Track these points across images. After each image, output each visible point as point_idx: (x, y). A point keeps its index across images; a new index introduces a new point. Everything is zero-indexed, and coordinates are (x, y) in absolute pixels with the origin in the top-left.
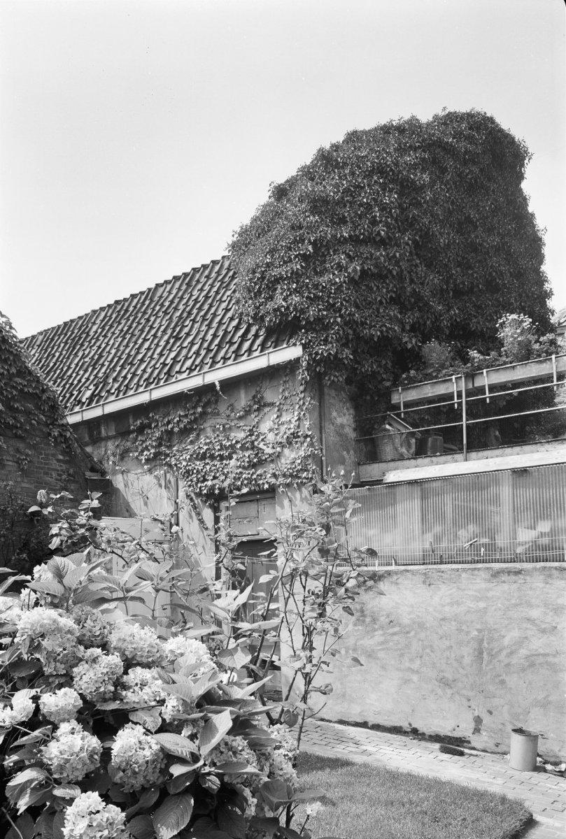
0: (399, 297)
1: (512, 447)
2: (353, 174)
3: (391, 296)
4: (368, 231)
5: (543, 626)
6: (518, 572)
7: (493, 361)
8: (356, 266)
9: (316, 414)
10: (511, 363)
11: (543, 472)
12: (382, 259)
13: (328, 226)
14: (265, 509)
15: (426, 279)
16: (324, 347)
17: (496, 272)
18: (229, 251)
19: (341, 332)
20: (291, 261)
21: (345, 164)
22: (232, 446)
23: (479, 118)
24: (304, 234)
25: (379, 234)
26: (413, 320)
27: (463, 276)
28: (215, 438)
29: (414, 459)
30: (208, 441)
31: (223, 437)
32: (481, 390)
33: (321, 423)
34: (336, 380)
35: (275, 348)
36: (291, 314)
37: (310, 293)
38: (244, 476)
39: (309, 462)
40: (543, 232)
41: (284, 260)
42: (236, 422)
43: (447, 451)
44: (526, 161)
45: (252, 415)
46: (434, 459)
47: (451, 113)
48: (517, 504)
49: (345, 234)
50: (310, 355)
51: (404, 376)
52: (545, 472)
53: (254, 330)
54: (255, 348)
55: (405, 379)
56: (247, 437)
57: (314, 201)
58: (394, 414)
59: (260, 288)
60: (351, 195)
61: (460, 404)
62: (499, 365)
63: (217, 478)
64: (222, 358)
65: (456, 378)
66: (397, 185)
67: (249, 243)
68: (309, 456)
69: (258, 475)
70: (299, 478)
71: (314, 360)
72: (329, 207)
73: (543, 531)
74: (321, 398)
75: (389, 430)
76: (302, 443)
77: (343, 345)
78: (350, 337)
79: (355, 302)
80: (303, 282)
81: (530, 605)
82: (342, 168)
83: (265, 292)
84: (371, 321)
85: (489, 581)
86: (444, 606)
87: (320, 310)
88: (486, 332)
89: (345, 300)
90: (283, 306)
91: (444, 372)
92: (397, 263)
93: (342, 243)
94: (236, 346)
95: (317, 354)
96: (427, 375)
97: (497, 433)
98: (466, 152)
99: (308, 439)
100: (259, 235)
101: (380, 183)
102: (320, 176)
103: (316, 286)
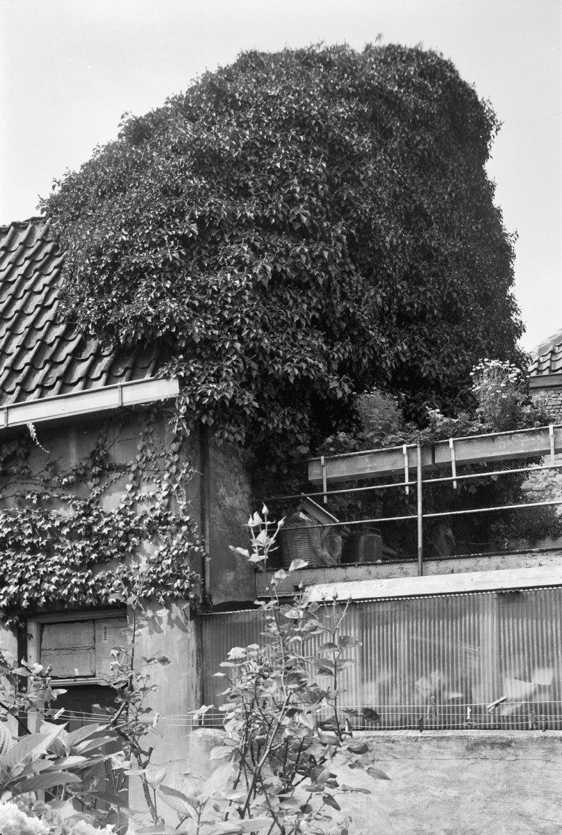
0: (324, 317)
1: (489, 556)
2: (258, 121)
3: (314, 316)
4: (282, 213)
5: (542, 825)
6: (506, 744)
7: (464, 427)
8: (264, 266)
9: (196, 489)
10: (489, 431)
11: (542, 596)
12: (304, 258)
13: (221, 197)
14: (109, 640)
15: (363, 295)
16: (215, 386)
17: (458, 294)
18: (43, 211)
19: (241, 365)
20: (162, 243)
21: (246, 105)
22: (55, 532)
23: (432, 61)
24: (184, 205)
25: (298, 219)
26: (343, 355)
27: (410, 295)
28: (23, 516)
29: (343, 567)
30: (11, 519)
31: (38, 515)
32: (445, 469)
33: (202, 504)
34: (231, 438)
35: (130, 379)
36: (161, 328)
37: (193, 298)
38: (73, 581)
39: (185, 565)
40: (513, 239)
41: (151, 242)
42: (60, 491)
43: (388, 559)
44: (493, 133)
45: (89, 483)
46: (372, 568)
47: (393, 46)
48: (505, 643)
49: (249, 214)
50: (192, 396)
51: (329, 440)
52: (545, 597)
53: (92, 346)
54: (96, 374)
55: (331, 445)
56: (80, 517)
57: (199, 155)
58: (311, 497)
59: (107, 280)
60: (257, 154)
61: (414, 487)
62: (472, 434)
63: (26, 581)
64: (38, 386)
65: (408, 448)
66: (325, 148)
67: (83, 204)
68: (185, 554)
69: (98, 581)
70: (168, 588)
71: (199, 404)
72: (224, 168)
73: (542, 684)
74: (204, 463)
75: (304, 520)
76: (173, 534)
77: (243, 385)
78: (254, 374)
79: (262, 319)
80: (183, 279)
81: (523, 794)
82: (242, 108)
83: (118, 289)
84: (285, 352)
85: (463, 757)
86: (394, 794)
87: (208, 328)
88: (444, 381)
89: (248, 316)
90: (149, 314)
91: (390, 437)
92: (325, 267)
93: (243, 226)
94: (63, 368)
95: (203, 395)
96: (363, 440)
97: (450, 532)
98: (416, 110)
99: (184, 528)
100: (104, 193)
101: (300, 141)
102: (207, 117)
103: (203, 289)
